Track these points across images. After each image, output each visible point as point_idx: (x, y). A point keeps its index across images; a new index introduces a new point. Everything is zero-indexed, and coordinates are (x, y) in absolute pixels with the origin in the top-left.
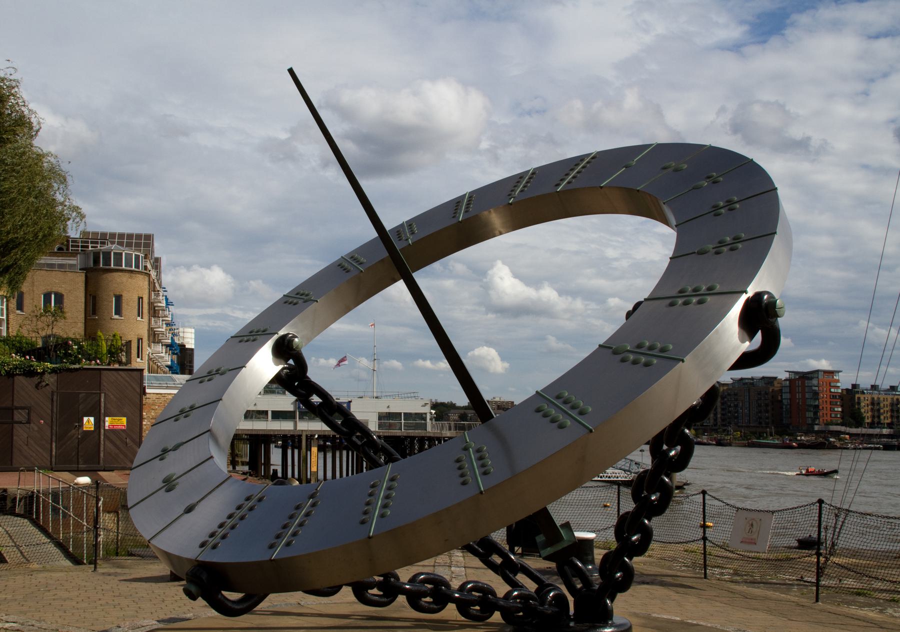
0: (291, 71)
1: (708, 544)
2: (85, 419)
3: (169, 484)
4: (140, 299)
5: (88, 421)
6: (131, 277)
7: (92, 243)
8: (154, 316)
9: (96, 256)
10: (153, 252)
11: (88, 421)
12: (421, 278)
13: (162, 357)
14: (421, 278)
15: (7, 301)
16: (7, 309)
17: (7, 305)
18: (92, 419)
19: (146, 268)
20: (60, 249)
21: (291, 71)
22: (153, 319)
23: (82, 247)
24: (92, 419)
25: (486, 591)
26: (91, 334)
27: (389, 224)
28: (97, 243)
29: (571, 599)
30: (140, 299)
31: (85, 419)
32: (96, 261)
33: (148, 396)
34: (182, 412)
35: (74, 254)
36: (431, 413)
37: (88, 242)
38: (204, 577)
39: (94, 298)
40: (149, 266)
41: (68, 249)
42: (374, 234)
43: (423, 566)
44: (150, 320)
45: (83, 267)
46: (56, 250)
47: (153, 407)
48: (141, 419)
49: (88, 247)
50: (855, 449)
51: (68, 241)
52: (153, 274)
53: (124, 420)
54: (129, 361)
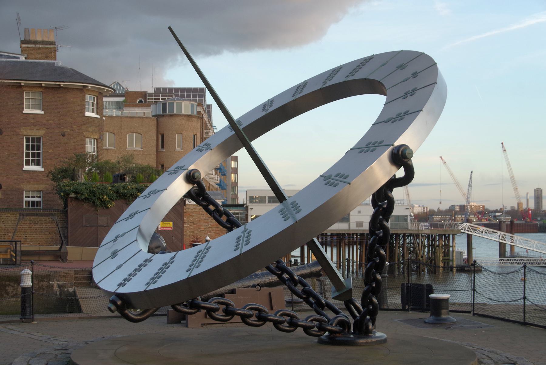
0: (170, 28)
1: (475, 292)
4: (195, 136)
6: (188, 120)
7: (162, 96)
10: (205, 100)
12: (255, 144)
13: (213, 178)
14: (255, 144)
15: (97, 142)
16: (97, 148)
17: (97, 145)
20: (140, 101)
21: (170, 28)
23: (155, 99)
27: (236, 116)
28: (165, 96)
32: (164, 109)
33: (187, 207)
35: (149, 106)
36: (411, 215)
38: (119, 303)
41: (145, 101)
42: (227, 123)
43: (51, 267)
45: (155, 114)
46: (138, 102)
47: (191, 214)
48: (183, 222)
49: (159, 99)
50: (417, 236)
51: (145, 96)
52: (205, 117)
53: (171, 223)
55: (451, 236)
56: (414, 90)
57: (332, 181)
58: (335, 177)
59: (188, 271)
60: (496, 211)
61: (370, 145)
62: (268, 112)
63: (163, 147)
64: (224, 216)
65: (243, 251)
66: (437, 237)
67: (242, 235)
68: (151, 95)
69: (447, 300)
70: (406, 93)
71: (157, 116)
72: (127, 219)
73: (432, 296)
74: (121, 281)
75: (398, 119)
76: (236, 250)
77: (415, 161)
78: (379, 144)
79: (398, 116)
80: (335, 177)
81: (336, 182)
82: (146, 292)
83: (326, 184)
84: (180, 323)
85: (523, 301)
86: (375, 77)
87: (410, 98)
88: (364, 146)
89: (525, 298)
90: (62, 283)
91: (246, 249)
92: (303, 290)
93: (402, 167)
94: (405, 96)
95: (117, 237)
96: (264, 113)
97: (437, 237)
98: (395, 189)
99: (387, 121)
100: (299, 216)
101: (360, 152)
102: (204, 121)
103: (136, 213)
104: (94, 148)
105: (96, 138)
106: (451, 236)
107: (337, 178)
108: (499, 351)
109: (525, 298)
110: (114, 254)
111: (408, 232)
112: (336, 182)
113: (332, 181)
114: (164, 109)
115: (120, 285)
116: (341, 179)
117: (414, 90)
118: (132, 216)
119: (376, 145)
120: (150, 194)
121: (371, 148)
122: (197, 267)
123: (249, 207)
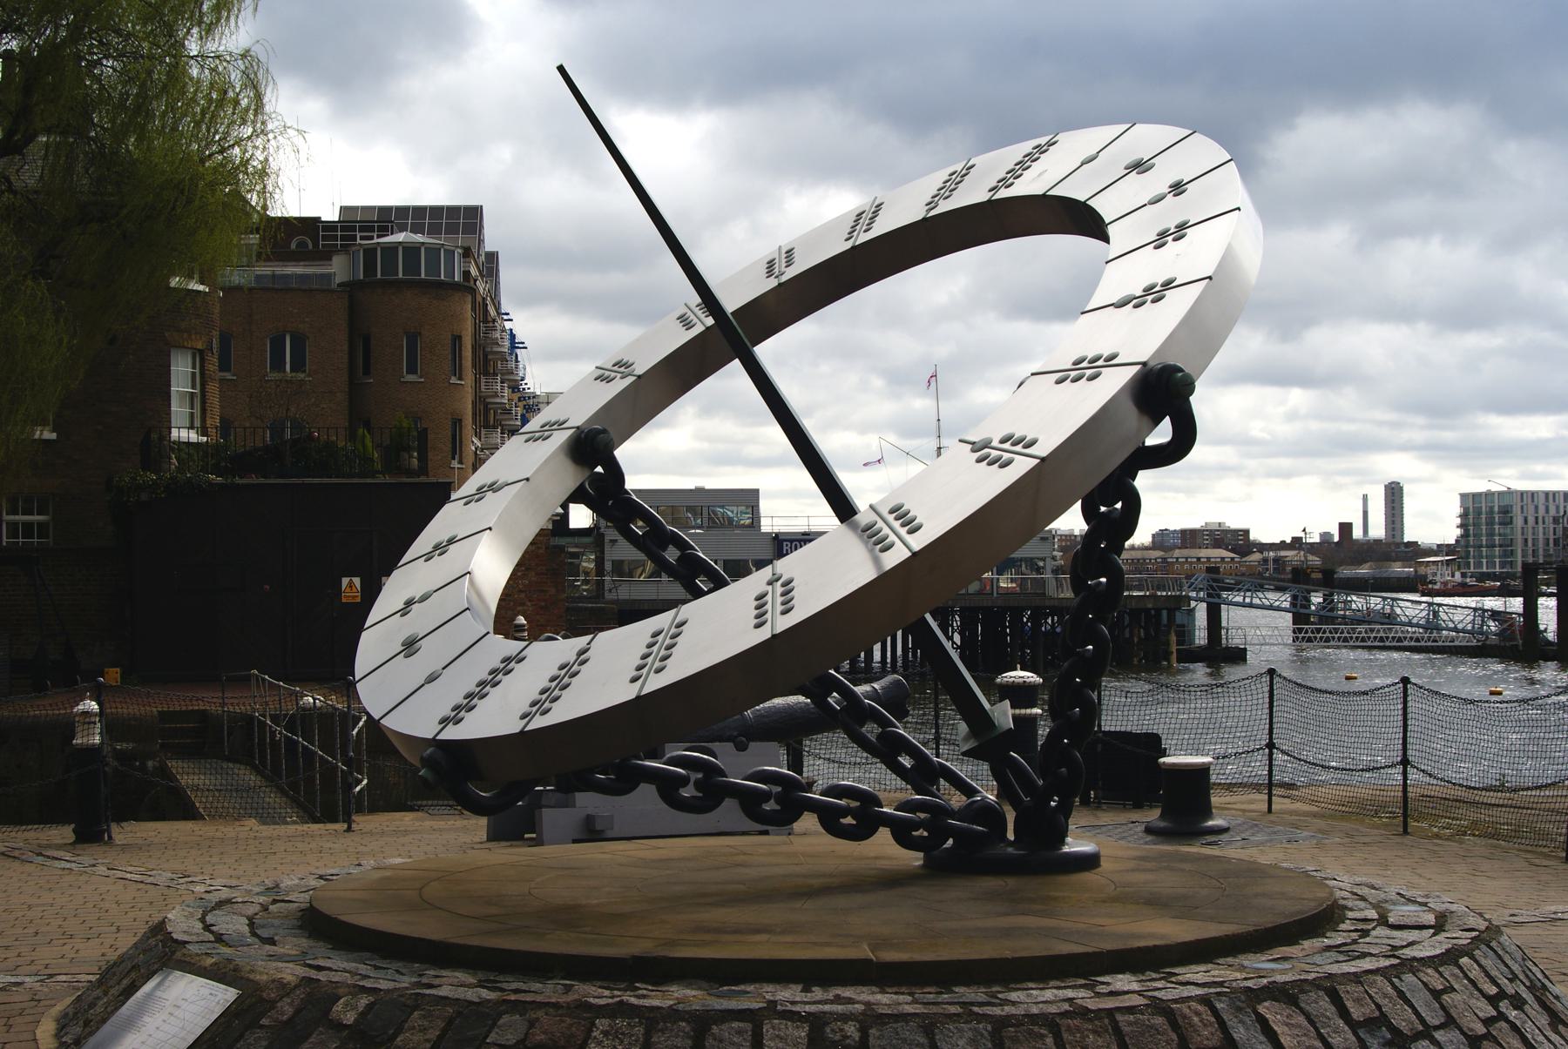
0: (561, 69)
1: (1278, 756)
2: (345, 581)
3: (410, 646)
5: (351, 584)
8: (486, 374)
9: (370, 253)
10: (481, 241)
11: (351, 584)
14: (765, 351)
18: (357, 581)
19: (467, 274)
20: (302, 244)
21: (561, 69)
22: (483, 380)
23: (343, 238)
24: (357, 581)
25: (868, 800)
26: (358, 418)
29: (1011, 816)
30: (457, 339)
31: (345, 581)
34: (436, 547)
37: (343, 238)
39: (367, 340)
40: (474, 271)
41: (316, 244)
44: (477, 382)
46: (293, 246)
52: (481, 286)
54: (423, 470)
55: (1165, 613)
56: (1182, 227)
57: (995, 453)
58: (1002, 442)
59: (634, 680)
60: (1283, 545)
61: (1084, 364)
62: (784, 279)
63: (367, 372)
64: (671, 548)
65: (779, 630)
66: (1127, 618)
67: (770, 588)
68: (330, 226)
69: (1203, 771)
70: (1163, 234)
71: (350, 287)
72: (428, 557)
73: (1162, 760)
74: (446, 711)
75: (1150, 298)
76: (757, 626)
77: (1200, 402)
78: (1107, 360)
79: (1148, 290)
80: (1002, 442)
81: (1006, 456)
82: (523, 739)
83: (979, 461)
84: (522, 839)
85: (1400, 768)
86: (1076, 191)
87: (1172, 246)
88: (1069, 366)
89: (1405, 762)
90: (131, 746)
91: (784, 623)
92: (879, 737)
93: (1167, 421)
94: (1161, 240)
95: (409, 603)
96: (772, 283)
97: (1127, 618)
98: (1141, 474)
99: (1120, 305)
100: (918, 542)
101: (1059, 382)
102: (479, 299)
103: (451, 541)
104: (193, 374)
105: (200, 346)
106: (1165, 613)
107: (1007, 446)
108: (1377, 882)
109: (1405, 762)
110: (410, 646)
111: (1047, 603)
112: (1006, 456)
113: (995, 453)
114: (370, 266)
115: (445, 721)
116: (1018, 448)
117: (1182, 227)
118: (440, 548)
119: (1100, 363)
120: (481, 491)
121: (1089, 372)
122: (658, 671)
123: (607, 539)
